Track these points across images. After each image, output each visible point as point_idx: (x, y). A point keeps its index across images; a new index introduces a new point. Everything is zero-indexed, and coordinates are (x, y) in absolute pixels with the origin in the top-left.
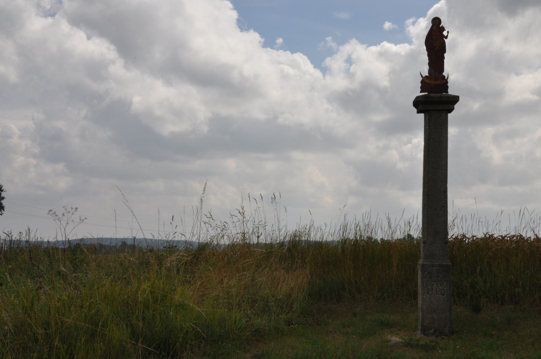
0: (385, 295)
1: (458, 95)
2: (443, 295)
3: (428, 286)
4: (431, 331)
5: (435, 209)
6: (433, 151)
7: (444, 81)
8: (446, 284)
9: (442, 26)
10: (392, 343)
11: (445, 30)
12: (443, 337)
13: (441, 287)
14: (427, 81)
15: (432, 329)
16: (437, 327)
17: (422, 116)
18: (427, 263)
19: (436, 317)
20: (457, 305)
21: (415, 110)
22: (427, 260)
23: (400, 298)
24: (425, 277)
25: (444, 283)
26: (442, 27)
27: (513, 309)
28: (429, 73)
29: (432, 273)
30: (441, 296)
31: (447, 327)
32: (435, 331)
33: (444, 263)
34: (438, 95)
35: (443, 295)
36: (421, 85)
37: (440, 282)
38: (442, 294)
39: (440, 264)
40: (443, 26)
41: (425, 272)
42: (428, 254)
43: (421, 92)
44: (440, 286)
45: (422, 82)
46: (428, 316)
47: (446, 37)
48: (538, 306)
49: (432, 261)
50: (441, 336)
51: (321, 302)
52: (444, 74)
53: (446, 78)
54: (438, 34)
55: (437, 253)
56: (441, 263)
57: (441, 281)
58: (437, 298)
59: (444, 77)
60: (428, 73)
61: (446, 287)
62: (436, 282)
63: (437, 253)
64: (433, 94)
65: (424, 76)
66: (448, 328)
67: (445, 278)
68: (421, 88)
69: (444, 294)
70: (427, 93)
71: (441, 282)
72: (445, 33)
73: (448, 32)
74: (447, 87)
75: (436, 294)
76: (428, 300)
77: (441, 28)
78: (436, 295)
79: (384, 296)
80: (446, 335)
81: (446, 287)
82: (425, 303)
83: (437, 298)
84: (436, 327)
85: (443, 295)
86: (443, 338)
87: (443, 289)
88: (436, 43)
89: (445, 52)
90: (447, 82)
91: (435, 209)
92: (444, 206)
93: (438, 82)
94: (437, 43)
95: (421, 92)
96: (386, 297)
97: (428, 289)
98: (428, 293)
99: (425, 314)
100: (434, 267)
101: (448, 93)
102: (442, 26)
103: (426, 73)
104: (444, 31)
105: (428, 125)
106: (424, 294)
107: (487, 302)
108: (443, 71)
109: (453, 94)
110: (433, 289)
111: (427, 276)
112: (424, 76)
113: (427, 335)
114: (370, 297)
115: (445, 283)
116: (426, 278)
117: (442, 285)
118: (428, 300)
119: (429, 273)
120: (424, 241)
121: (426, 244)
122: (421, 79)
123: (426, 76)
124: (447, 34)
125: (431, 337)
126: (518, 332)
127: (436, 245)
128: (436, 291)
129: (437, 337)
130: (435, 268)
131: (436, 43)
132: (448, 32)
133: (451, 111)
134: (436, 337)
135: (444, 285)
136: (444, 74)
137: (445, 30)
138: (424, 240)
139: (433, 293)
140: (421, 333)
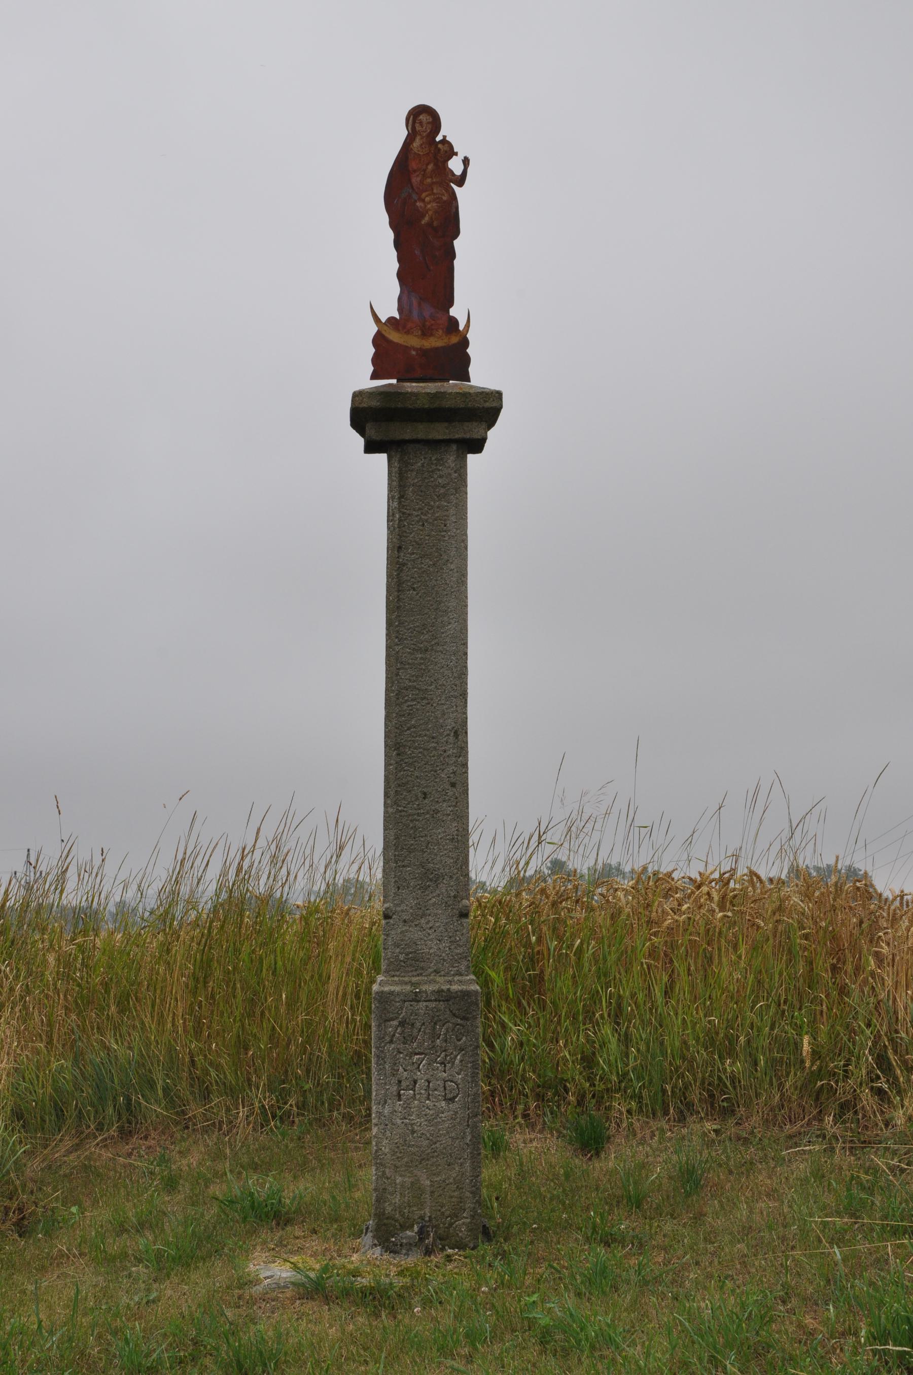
0: (292, 1101)
1: (497, 389)
2: (452, 1100)
3: (401, 1069)
4: (409, 1233)
5: (425, 795)
6: (414, 589)
7: (455, 340)
8: (461, 1061)
9: (445, 137)
10: (257, 1290)
11: (456, 154)
12: (450, 1251)
13: (445, 1071)
14: (394, 336)
15: (412, 1226)
16: (430, 1217)
17: (381, 459)
18: (397, 989)
19: (428, 1183)
20: (532, 1126)
21: (360, 441)
22: (396, 979)
23: (342, 1110)
24: (388, 1039)
25: (456, 1056)
26: (444, 141)
27: (713, 1135)
28: (400, 310)
29: (413, 1025)
30: (443, 1104)
31: (465, 1215)
32: (421, 1232)
33: (455, 987)
34: (431, 387)
35: (452, 1100)
36: (372, 350)
37: (443, 1055)
38: (449, 1096)
39: (440, 991)
40: (448, 139)
41: (389, 1021)
42: (402, 957)
43: (374, 376)
44: (441, 1068)
45: (378, 340)
46: (399, 1180)
47: (461, 181)
48: (793, 1120)
49: (414, 979)
50: (443, 1249)
51: (61, 1140)
52: (453, 312)
53: (461, 327)
54: (430, 167)
55: (432, 951)
56: (445, 987)
57: (445, 1051)
58: (431, 1112)
59: (454, 322)
60: (398, 310)
61: (461, 1070)
62: (426, 1055)
63: (432, 951)
64: (414, 384)
65: (383, 320)
66: (469, 1220)
67: (459, 1040)
68: (375, 360)
69: (456, 1097)
70: (394, 381)
71: (446, 1056)
72: (455, 166)
73: (466, 161)
74: (467, 360)
75: (428, 1099)
76: (399, 1121)
77: (440, 146)
78: (427, 1102)
79: (287, 1106)
80: (461, 1246)
81: (461, 1070)
82: (388, 1134)
83: (431, 1112)
84: (427, 1219)
85: (450, 1099)
86: (449, 1258)
87: (452, 1081)
88: (423, 201)
89: (456, 233)
90: (465, 343)
91: (425, 795)
92: (453, 785)
93: (434, 342)
94: (427, 199)
95: (374, 376)
96: (295, 1109)
97: (400, 1082)
98: (399, 1095)
99: (387, 1170)
100: (418, 1001)
101: (468, 380)
102: (445, 137)
103: (389, 309)
104: (450, 158)
105: (397, 495)
106: (385, 1102)
107: (629, 1112)
108: (451, 303)
109: (481, 386)
110: (415, 1082)
111: (397, 1035)
112: (383, 320)
113: (392, 1249)
114: (238, 1113)
115: (459, 1057)
116: (391, 1042)
117: (448, 1066)
118: (399, 1121)
119: (402, 1024)
120: (387, 909)
121: (391, 921)
122: (374, 329)
123: (391, 320)
124: (462, 167)
125: (408, 1255)
126: (570, 1301)
127: (428, 923)
128: (428, 1086)
129: (428, 1252)
130: (422, 1005)
131: (423, 201)
132: (466, 161)
133: (477, 446)
134: (425, 1254)
135: (453, 1063)
136: (453, 312)
137: (456, 154)
138: (386, 905)
139: (418, 1097)
140: (376, 1242)
